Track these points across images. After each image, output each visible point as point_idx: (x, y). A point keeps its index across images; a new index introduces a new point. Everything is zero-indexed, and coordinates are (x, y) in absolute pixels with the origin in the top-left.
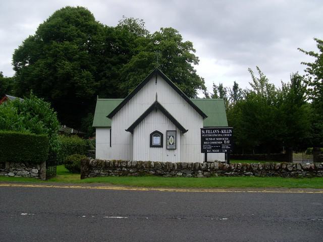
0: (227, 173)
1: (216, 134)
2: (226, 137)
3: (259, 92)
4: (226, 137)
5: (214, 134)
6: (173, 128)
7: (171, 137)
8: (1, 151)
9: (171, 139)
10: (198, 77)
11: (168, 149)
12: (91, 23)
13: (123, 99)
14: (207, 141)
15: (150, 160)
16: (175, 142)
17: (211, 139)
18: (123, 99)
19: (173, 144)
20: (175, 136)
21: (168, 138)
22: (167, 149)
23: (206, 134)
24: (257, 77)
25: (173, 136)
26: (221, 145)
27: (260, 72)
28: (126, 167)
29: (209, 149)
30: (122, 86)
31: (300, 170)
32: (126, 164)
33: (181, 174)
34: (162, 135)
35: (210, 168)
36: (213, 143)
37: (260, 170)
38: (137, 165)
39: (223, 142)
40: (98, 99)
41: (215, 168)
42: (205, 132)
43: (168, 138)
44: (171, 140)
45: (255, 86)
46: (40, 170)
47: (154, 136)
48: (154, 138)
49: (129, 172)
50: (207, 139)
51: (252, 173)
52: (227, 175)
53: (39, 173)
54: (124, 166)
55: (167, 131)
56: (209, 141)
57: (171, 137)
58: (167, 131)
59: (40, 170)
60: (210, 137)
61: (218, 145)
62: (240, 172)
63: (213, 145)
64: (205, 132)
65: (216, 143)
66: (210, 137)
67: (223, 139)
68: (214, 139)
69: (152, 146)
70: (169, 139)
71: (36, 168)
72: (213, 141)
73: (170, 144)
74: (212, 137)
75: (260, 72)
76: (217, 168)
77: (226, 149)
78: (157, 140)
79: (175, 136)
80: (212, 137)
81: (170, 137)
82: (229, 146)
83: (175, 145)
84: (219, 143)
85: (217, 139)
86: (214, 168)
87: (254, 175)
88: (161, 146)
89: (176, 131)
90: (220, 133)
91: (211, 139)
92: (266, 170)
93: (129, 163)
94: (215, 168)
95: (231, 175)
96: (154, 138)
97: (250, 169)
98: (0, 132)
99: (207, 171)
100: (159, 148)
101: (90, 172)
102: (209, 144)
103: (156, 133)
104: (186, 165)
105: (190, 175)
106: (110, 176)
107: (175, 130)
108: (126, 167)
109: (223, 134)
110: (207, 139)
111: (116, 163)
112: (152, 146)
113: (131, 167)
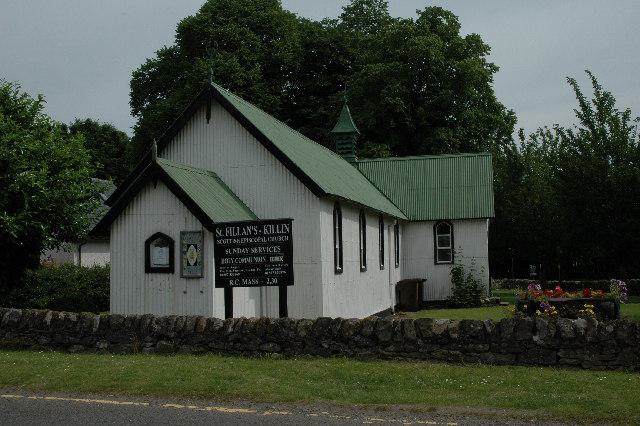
2: (275, 244)
4: (275, 244)
7: (192, 247)
8: (630, 311)
10: (496, 108)
12: (390, 30)
14: (227, 256)
17: (239, 251)
22: (182, 277)
24: (589, 96)
25: (196, 246)
26: (262, 266)
29: (234, 278)
31: (414, 342)
35: (174, 330)
42: (224, 233)
45: (585, 116)
50: (228, 252)
56: (235, 256)
57: (192, 247)
58: (183, 234)
62: (560, 352)
63: (243, 266)
64: (224, 233)
67: (268, 249)
69: (149, 269)
70: (185, 253)
72: (242, 256)
78: (160, 256)
81: (189, 246)
84: (258, 260)
85: (254, 251)
88: (170, 269)
90: (262, 235)
91: (239, 251)
99: (169, 339)
103: (160, 239)
104: (121, 320)
110: (228, 252)
112: (149, 269)
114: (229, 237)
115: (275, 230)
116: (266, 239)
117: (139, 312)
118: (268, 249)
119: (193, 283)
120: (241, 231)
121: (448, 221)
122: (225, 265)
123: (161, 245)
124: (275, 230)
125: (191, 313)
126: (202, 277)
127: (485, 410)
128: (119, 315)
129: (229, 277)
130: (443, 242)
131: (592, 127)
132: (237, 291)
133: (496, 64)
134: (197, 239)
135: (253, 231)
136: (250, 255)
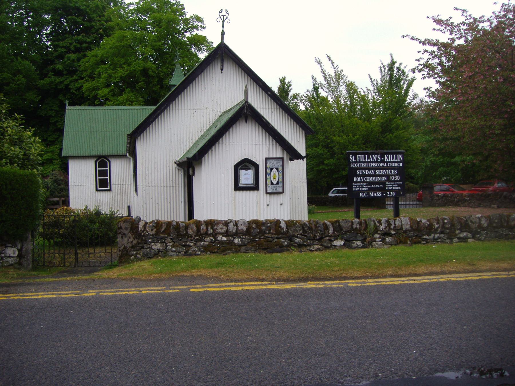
0: (426, 237)
1: (374, 162)
3: (19, 30)
5: (371, 162)
6: (277, 152)
7: (274, 170)
9: (275, 174)
11: (270, 194)
13: (154, 108)
14: (359, 176)
15: (279, 219)
16: (281, 180)
17: (367, 172)
18: (154, 108)
19: (277, 183)
20: (280, 169)
21: (268, 171)
23: (356, 162)
25: (277, 169)
26: (383, 183)
27: (333, 63)
28: (227, 234)
30: (87, 85)
32: (225, 229)
33: (342, 243)
34: (256, 167)
36: (371, 179)
37: (483, 229)
38: (249, 228)
39: (389, 180)
40: (68, 108)
41: (404, 228)
42: (356, 158)
43: (268, 171)
44: (275, 176)
46: (22, 248)
47: (242, 169)
48: (242, 173)
49: (231, 243)
50: (359, 172)
51: (470, 235)
52: (426, 240)
53: (20, 256)
54: (222, 231)
55: (266, 159)
56: (364, 176)
57: (274, 170)
58: (266, 159)
59: (22, 248)
60: (365, 169)
61: (379, 183)
63: (370, 183)
64: (356, 158)
65: (375, 179)
66: (365, 169)
67: (388, 172)
68: (372, 172)
69: (237, 187)
70: (270, 174)
71: (14, 245)
73: (272, 183)
74: (369, 169)
75: (333, 63)
76: (408, 227)
77: (392, 190)
79: (280, 169)
80: (369, 169)
81: (272, 169)
82: (399, 185)
83: (280, 185)
84: (381, 179)
85: (378, 172)
86: (401, 228)
87: (473, 237)
88: (255, 187)
89: (282, 159)
90: (383, 161)
91: (367, 172)
92: (495, 228)
93: (231, 225)
94: (404, 228)
95: (435, 240)
96: (242, 173)
97: (465, 226)
98: (0, 168)
100: (252, 192)
101: (143, 247)
102: (364, 182)
105: (359, 243)
106: (190, 255)
107: (279, 155)
108: (227, 234)
109: (387, 162)
111: (203, 227)
112: (237, 187)
113: (237, 234)
114: (360, 162)
115: (393, 158)
116: (387, 164)
117: (209, 219)
118: (388, 172)
119: (275, 198)
120: (368, 158)
121: (106, 157)
122: (356, 182)
123: (247, 168)
124: (393, 158)
125: (271, 217)
126: (283, 192)
127: (49, 346)
128: (289, 220)
129: (359, 191)
130: (103, 173)
131: (155, 73)
132: (126, 214)
133: (412, 40)
134: (279, 164)
135: (377, 159)
136: (375, 175)
